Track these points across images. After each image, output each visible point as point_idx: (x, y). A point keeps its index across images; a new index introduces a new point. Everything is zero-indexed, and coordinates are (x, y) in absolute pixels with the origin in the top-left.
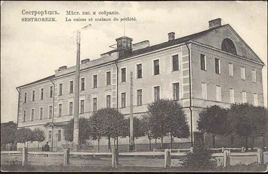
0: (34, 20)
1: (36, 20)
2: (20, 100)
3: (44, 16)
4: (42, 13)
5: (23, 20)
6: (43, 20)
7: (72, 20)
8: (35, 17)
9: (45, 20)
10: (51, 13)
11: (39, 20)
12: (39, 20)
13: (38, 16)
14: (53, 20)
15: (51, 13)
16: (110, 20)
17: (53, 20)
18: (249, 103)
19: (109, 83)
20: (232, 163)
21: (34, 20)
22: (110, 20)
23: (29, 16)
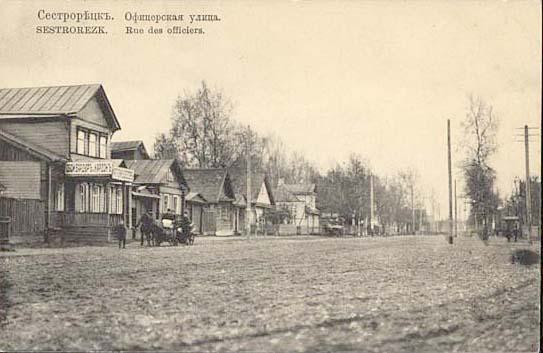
0: (61, 31)
1: (66, 31)
2: (220, 337)
3: (83, 23)
4: (78, 17)
5: (39, 30)
6: (80, 31)
7: (146, 31)
8: (64, 25)
9: (84, 30)
10: (98, 17)
11: (73, 30)
12: (73, 30)
13: (71, 23)
14: (201, 31)
15: (98, 17)
16: (141, 31)
17: (101, 31)
18: (469, 168)
19: (309, 304)
20: (536, 235)
21: (61, 31)
22: (141, 31)
23: (51, 23)
